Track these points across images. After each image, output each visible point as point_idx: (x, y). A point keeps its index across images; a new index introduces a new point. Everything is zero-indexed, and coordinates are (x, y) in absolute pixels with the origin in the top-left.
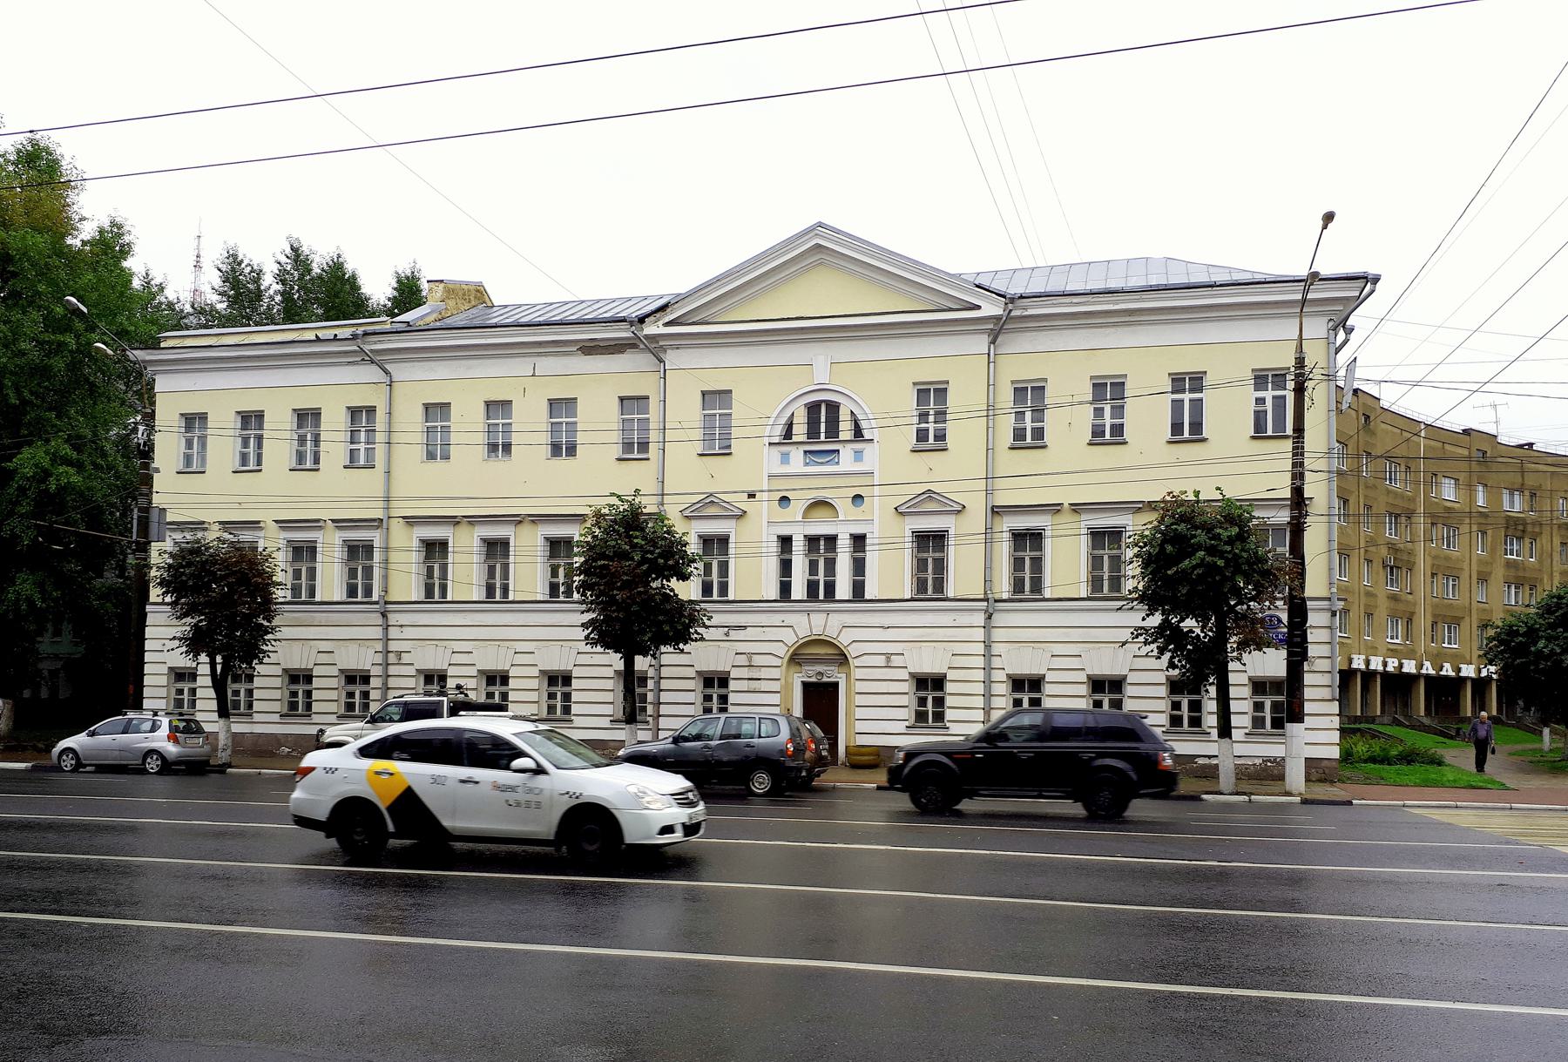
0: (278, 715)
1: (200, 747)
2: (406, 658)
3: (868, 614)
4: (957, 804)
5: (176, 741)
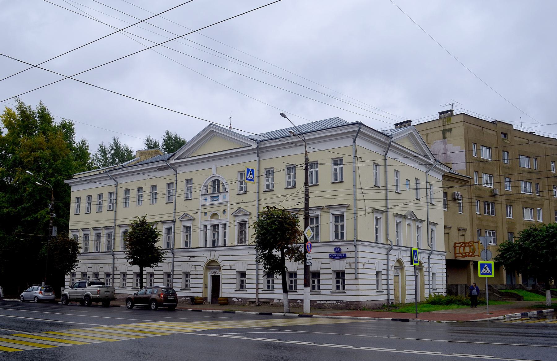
1: (51, 295)
2: (118, 269)
3: (228, 251)
5: (42, 294)
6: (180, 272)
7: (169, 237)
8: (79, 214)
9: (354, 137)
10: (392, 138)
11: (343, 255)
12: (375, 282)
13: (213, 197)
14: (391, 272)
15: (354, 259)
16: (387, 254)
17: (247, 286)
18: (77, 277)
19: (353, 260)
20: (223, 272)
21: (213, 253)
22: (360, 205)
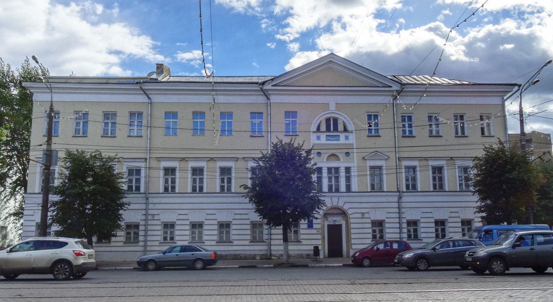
4: (545, 271)
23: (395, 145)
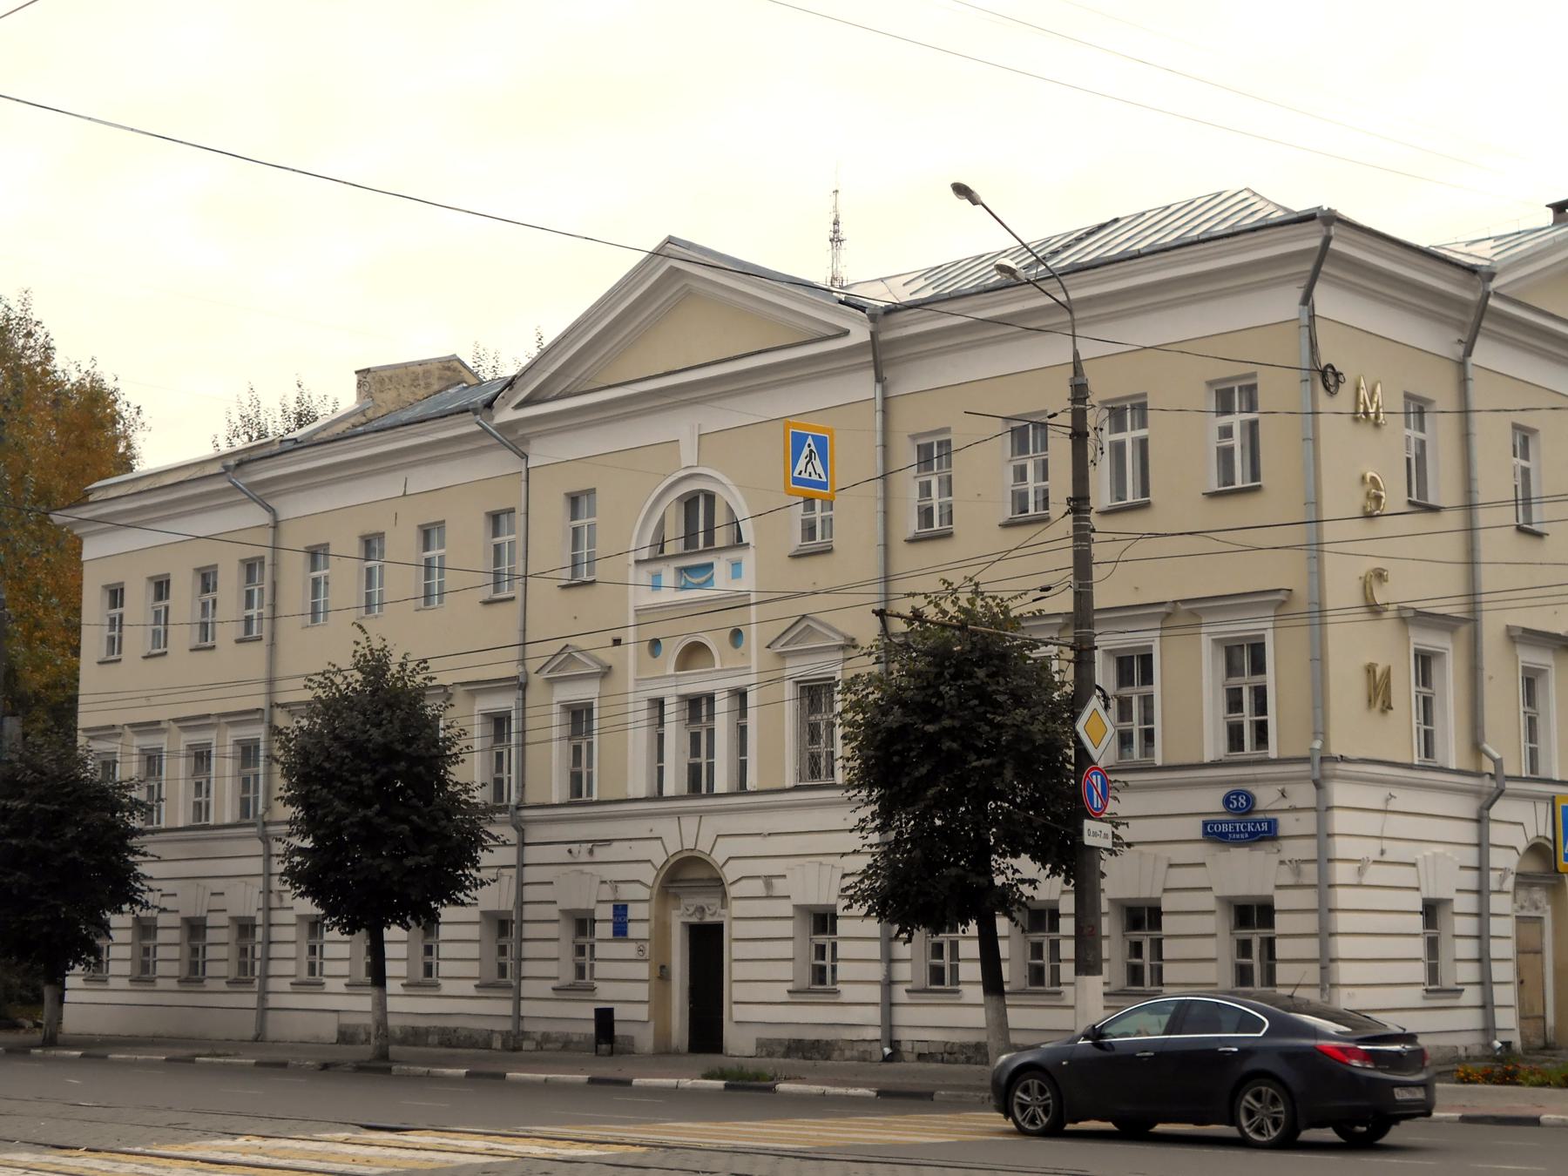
0: (176, 980)
4: (1377, 1140)
6: (552, 912)
7: (499, 756)
8: (120, 660)
9: (1304, 283)
10: (1491, 276)
11: (1265, 827)
12: (1418, 947)
13: (686, 569)
14: (1499, 903)
15: (1313, 842)
16: (1481, 820)
17: (843, 970)
18: (162, 936)
19: (1307, 849)
20: (737, 908)
21: (689, 824)
22: (1341, 588)
23: (1516, 496)
